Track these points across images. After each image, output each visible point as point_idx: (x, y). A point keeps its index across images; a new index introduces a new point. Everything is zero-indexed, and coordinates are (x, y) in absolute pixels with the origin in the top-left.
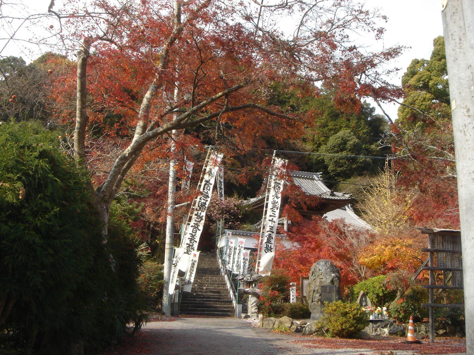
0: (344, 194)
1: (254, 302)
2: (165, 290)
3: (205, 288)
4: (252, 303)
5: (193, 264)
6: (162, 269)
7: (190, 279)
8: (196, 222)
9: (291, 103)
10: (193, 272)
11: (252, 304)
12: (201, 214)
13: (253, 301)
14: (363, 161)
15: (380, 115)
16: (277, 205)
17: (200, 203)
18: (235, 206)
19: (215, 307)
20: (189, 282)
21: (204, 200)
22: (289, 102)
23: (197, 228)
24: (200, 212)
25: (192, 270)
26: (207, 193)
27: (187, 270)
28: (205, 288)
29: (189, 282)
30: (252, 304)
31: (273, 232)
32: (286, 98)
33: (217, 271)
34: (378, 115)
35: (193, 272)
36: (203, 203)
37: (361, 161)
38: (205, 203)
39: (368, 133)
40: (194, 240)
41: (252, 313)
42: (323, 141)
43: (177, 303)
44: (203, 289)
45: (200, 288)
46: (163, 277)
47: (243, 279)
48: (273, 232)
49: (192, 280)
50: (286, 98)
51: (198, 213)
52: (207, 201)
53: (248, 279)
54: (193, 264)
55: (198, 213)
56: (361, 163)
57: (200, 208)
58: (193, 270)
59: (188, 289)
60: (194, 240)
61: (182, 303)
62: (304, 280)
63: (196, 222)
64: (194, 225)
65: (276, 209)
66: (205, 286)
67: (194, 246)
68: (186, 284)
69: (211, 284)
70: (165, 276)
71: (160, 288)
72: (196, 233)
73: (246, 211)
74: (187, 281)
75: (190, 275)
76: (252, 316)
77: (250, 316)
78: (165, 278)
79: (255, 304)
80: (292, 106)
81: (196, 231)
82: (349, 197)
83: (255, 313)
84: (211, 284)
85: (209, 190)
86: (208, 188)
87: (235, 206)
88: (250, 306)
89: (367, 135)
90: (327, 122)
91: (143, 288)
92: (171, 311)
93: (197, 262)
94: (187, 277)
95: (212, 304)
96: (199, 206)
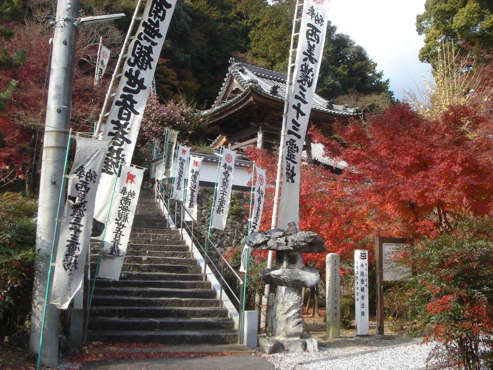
0: (346, 107)
1: (295, 306)
2: (37, 282)
3: (144, 258)
4: (287, 308)
5: (126, 200)
6: (32, 213)
7: (116, 242)
8: (127, 94)
9: (238, 9)
10: (126, 224)
11: (289, 310)
12: (138, 73)
13: (291, 303)
14: (331, 84)
15: (344, 35)
16: (310, 75)
17: (138, 46)
18: (182, 114)
19: (180, 314)
20: (114, 251)
21: (149, 41)
22: (236, 8)
23: (131, 107)
24: (135, 68)
25: (121, 218)
26: (157, 25)
27: (108, 216)
28: (144, 258)
29: (114, 251)
30: (289, 310)
31: (299, 137)
32: (232, 3)
33: (159, 221)
34: (342, 34)
35: (126, 224)
36: (146, 47)
37: (329, 84)
38: (150, 50)
39: (333, 53)
40: (122, 137)
41: (289, 336)
42: (279, 58)
43: (78, 311)
44: (140, 261)
45: (136, 260)
46: (35, 238)
47: (265, 243)
48: (299, 137)
49: (123, 247)
50: (232, 3)
51: (131, 70)
52: (154, 44)
53: (279, 244)
54: (126, 200)
55: (131, 70)
56: (328, 86)
57: (137, 60)
58: (126, 219)
59: (113, 270)
60: (122, 137)
61: (95, 303)
62: (384, 244)
63: (127, 94)
64: (121, 100)
65: (307, 85)
66: (144, 254)
67: (123, 152)
68: (105, 256)
69: (156, 248)
70: (39, 234)
71: (21, 276)
72: (128, 119)
73: (200, 123)
74: (107, 248)
75: (118, 233)
76: (290, 344)
77: (285, 344)
78: (38, 241)
79: (294, 311)
80: (239, 14)
81: (129, 115)
82: (354, 113)
83: (296, 335)
84: (156, 248)
85: (163, 19)
86: (161, 14)
87: (182, 114)
88: (281, 317)
89: (332, 55)
90: (284, 35)
91: (427, 115)
92: (60, 341)
93: (137, 196)
94: (108, 236)
95: (169, 302)
96: (133, 55)
